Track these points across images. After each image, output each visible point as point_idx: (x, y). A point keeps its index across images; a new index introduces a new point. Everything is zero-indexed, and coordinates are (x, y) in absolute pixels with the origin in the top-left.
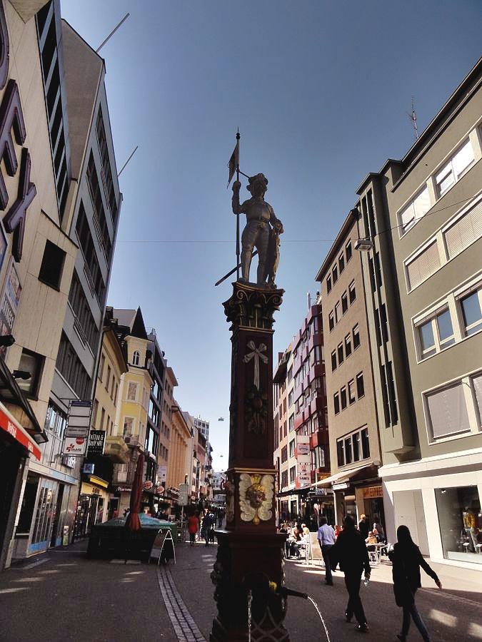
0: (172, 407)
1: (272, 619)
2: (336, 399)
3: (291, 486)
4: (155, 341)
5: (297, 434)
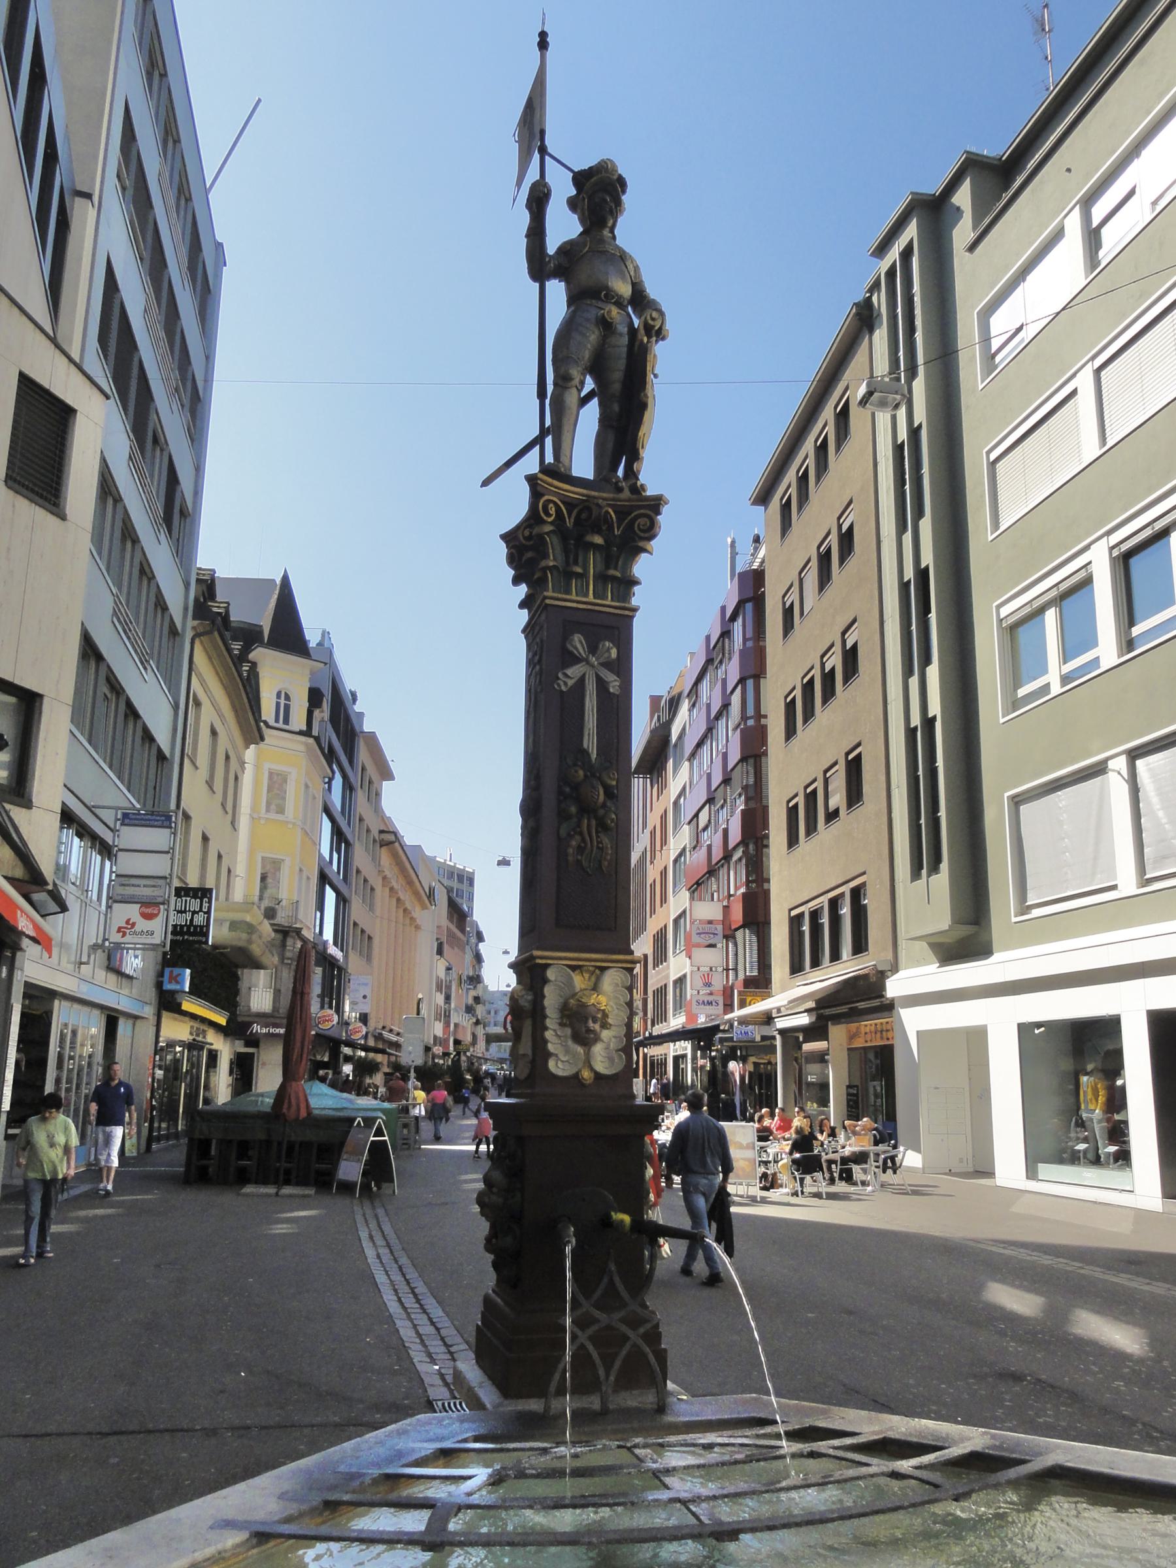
0: (381, 832)
1: (621, 1287)
2: (792, 812)
3: (676, 1022)
4: (329, 661)
5: (692, 899)
